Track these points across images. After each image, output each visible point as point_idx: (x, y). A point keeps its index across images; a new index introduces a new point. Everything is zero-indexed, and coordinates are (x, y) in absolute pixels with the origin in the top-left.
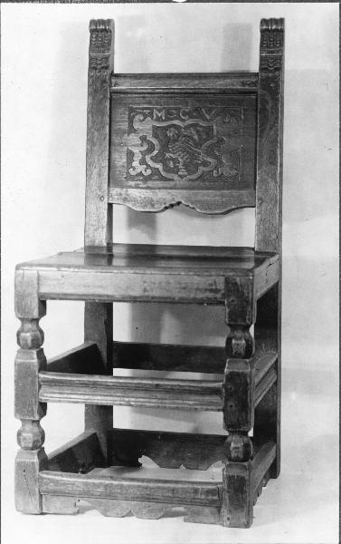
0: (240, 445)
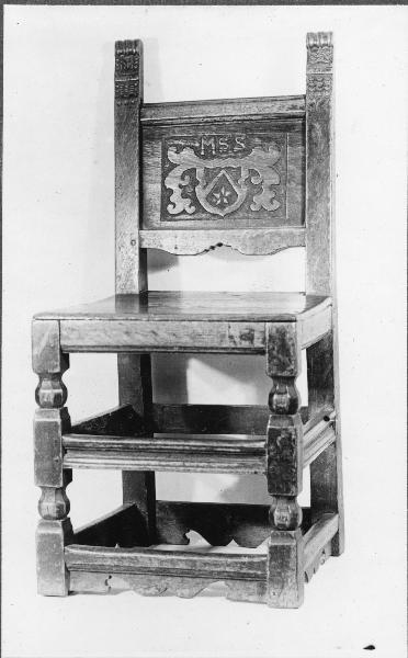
0: (287, 515)
